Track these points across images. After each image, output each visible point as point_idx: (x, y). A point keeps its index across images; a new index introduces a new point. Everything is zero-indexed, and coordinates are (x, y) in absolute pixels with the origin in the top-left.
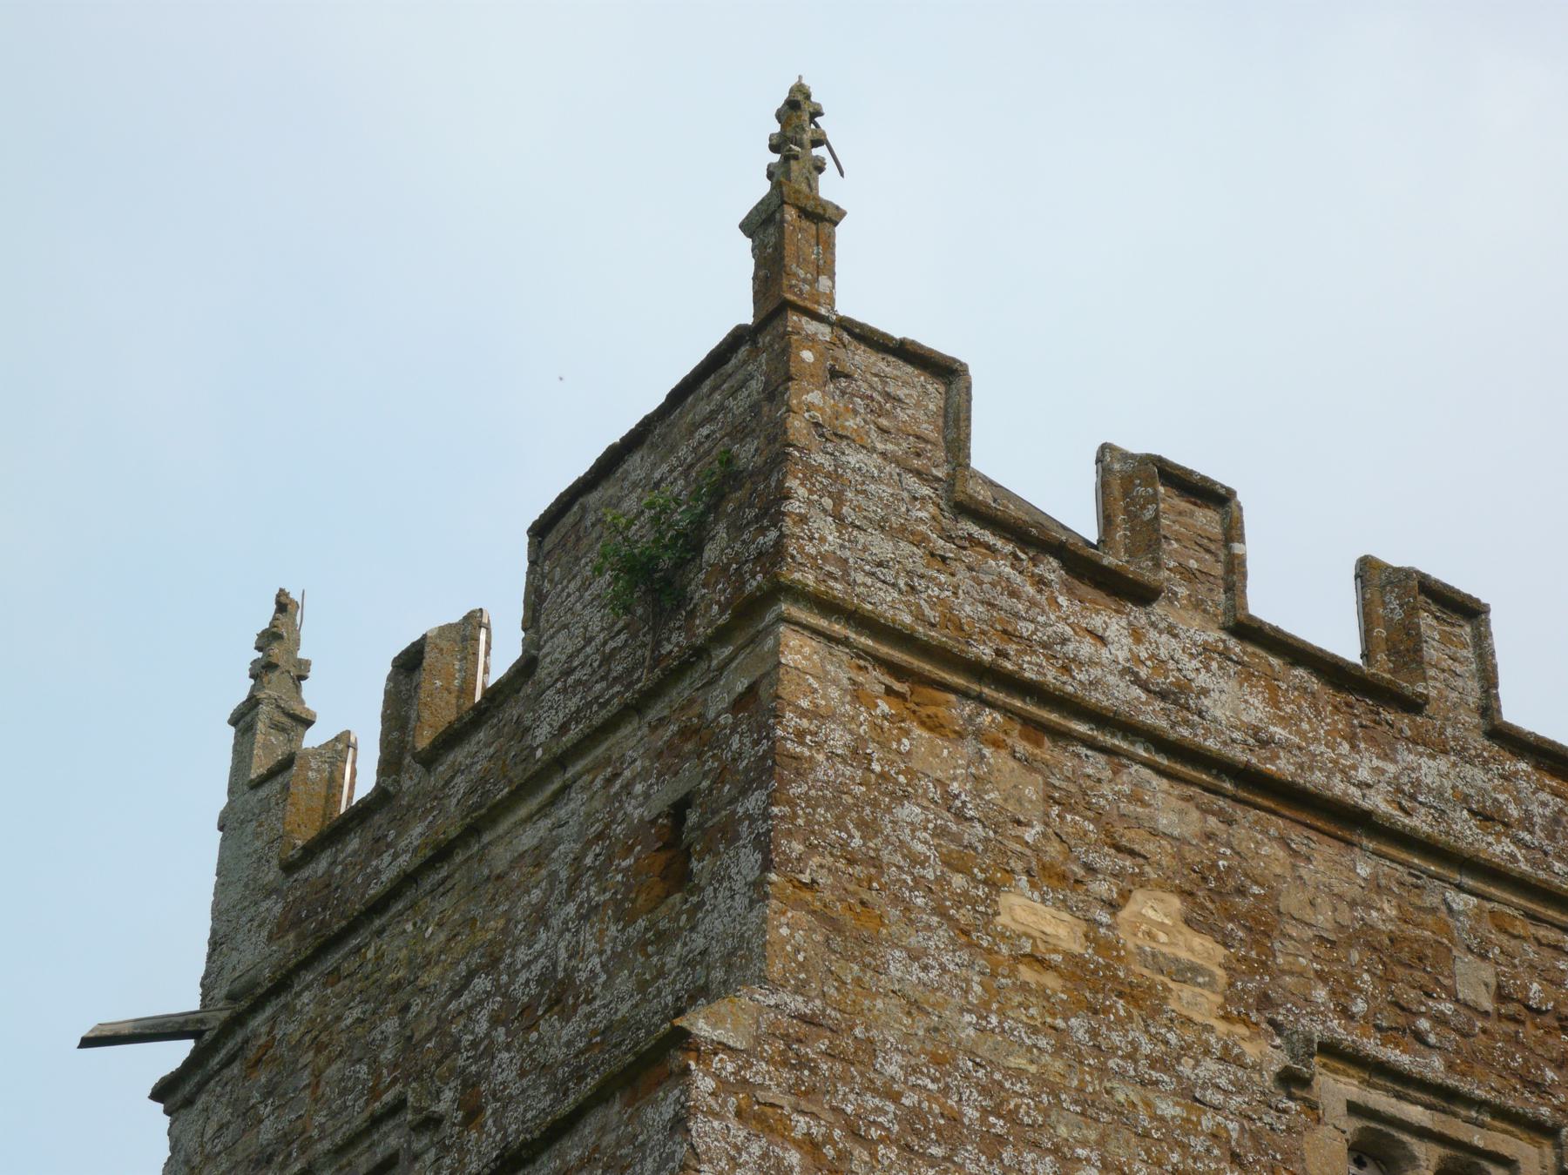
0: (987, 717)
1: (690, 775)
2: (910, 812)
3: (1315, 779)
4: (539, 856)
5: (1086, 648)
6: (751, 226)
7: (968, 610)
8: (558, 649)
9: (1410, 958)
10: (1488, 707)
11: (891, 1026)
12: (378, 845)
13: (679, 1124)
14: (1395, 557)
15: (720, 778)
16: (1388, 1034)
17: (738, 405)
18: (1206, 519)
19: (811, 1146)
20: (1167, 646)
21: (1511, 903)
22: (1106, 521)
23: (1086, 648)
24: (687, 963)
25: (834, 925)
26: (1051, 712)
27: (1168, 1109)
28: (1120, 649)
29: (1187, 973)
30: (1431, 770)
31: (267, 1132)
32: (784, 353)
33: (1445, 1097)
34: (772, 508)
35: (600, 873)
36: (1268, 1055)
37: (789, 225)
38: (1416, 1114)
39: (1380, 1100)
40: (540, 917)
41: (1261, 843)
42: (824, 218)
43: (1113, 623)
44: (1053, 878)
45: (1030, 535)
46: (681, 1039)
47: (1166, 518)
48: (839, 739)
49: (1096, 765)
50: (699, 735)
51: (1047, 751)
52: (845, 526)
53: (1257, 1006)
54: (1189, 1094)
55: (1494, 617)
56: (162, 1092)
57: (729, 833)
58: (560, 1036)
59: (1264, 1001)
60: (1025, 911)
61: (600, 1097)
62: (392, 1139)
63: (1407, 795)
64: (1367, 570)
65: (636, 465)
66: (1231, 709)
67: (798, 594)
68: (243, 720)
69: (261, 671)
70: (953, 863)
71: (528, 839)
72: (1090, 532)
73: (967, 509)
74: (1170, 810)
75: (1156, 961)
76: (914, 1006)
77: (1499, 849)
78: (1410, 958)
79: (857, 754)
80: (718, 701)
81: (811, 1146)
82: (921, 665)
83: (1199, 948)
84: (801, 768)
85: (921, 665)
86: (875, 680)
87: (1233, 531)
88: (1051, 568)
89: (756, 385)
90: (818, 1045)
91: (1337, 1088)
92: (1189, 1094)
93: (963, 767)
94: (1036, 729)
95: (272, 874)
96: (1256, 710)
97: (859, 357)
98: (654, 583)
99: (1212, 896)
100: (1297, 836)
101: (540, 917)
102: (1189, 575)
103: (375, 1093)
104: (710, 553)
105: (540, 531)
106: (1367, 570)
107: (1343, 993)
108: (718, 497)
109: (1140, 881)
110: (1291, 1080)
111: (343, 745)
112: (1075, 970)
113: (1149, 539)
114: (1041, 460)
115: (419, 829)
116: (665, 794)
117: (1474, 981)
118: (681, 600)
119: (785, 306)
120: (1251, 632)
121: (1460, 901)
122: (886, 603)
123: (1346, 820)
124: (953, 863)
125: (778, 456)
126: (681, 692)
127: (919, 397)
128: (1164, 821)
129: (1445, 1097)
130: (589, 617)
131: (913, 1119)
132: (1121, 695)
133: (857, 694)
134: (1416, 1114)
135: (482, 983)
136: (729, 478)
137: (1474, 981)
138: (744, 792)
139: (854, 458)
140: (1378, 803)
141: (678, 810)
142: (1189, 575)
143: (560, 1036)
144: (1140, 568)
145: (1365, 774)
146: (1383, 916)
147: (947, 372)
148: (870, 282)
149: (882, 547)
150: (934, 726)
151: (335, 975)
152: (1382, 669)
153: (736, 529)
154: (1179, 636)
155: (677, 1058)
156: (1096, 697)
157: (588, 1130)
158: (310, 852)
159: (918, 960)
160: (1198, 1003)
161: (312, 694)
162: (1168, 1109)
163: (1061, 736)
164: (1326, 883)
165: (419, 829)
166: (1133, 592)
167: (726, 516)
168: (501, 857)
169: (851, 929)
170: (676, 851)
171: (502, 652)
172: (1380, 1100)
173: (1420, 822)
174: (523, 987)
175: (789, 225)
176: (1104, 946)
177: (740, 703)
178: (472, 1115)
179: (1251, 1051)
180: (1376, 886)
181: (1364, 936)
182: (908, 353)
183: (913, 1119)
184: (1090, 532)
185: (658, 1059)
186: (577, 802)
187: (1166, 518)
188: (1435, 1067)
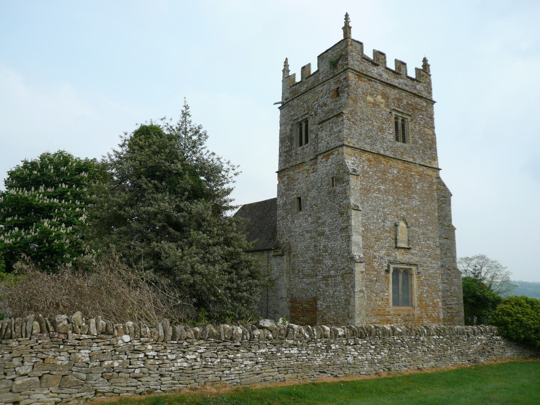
0: (366, 79)
1: (338, 85)
2: (360, 89)
3: (392, 83)
4: (322, 91)
5: (373, 71)
6: (343, 28)
7: (364, 68)
8: (321, 70)
9: (399, 100)
10: (406, 74)
11: (359, 110)
12: (301, 86)
13: (342, 120)
14: (399, 59)
15: (342, 86)
16: (398, 107)
17: (342, 47)
18: (383, 56)
19: (353, 122)
20: (380, 70)
21: (408, 94)
22: (374, 57)
23: (373, 71)
24: (339, 104)
25: (354, 101)
26: (370, 78)
27: (381, 116)
28: (376, 71)
29: (382, 103)
30: (401, 81)
31: (292, 113)
32: (347, 43)
33: (402, 113)
34: (347, 59)
35: (329, 94)
36: (388, 110)
37: (347, 29)
38: (400, 115)
39: (397, 114)
40: (322, 97)
41: (388, 90)
42: (350, 28)
43: (375, 68)
44: (371, 95)
45: (368, 60)
46: (342, 113)
47: (380, 56)
48: (354, 83)
49: (374, 83)
50: (339, 81)
51: (370, 82)
52: (353, 62)
53: (387, 106)
54: (382, 114)
55: (408, 65)
56: (279, 108)
57: (344, 92)
58: (326, 109)
59: (388, 105)
60: (369, 98)
61: (334, 117)
62: (307, 116)
63: (399, 84)
64: (396, 60)
65: (330, 52)
66: (385, 76)
67: (350, 69)
68: (284, 71)
69: (285, 66)
70: (363, 94)
71: (320, 89)
72: (372, 59)
73: (363, 58)
74: (380, 87)
75: (380, 102)
76: (361, 108)
77: (407, 88)
78: (399, 100)
79: (355, 84)
80: (341, 78)
81: (353, 122)
82: (361, 75)
83: (383, 101)
84: (351, 86)
85: (361, 75)
86: (356, 76)
87: (385, 58)
88: (370, 63)
89: (344, 46)
90: (353, 112)
91: (394, 113)
92: (382, 114)
93: (364, 85)
94: (369, 80)
95: (289, 87)
96: (387, 76)
97: (354, 43)
98: (334, 64)
99: (385, 96)
100: (391, 89)
101: (322, 97)
102: (382, 63)
103: (304, 111)
104: (339, 63)
105: (318, 57)
106: (396, 60)
107: (394, 104)
108: (340, 58)
109: (378, 94)
110: (390, 113)
111: (294, 75)
112: (373, 104)
113: (378, 59)
114: (369, 53)
115: (306, 85)
116: (336, 87)
117: (405, 102)
118: (336, 67)
119: (347, 38)
120: (387, 68)
121: (404, 94)
122: (357, 69)
123: (395, 87)
124: (363, 94)
125: (347, 54)
126: (337, 77)
127: (358, 46)
128: (380, 88)
129: (402, 113)
130: (326, 66)
131: (360, 118)
132: (376, 76)
133: (355, 78)
134: (400, 115)
135: (316, 102)
136: (341, 56)
137: (405, 102)
138: (345, 88)
139: (354, 54)
140: (397, 85)
141: (338, 89)
142: (382, 63)
143: (326, 109)
144: (377, 63)
145: (396, 82)
146: (397, 96)
147: (361, 44)
148: (354, 35)
149: (356, 63)
150: (361, 80)
151: (298, 99)
152: (397, 71)
153: (342, 61)
154: (381, 69)
155: (342, 114)
156: (374, 77)
157: (332, 119)
158: (293, 86)
159: (361, 104)
160: (383, 106)
161: (290, 68)
162: (381, 116)
163: (371, 81)
164: (393, 93)
165: (306, 85)
166: (376, 65)
167: (341, 58)
168: (317, 90)
169: (355, 101)
170: (338, 93)
171: (314, 69)
172: (397, 114)
173: (400, 86)
174: (321, 103)
175: (347, 29)
176: (375, 101)
177: (344, 79)
178: (316, 115)
179: (387, 110)
180: (397, 93)
181: (396, 98)
182: (358, 42)
183: (360, 118)
184: (372, 59)
185: (340, 114)
186: (325, 86)
187: (380, 56)
188: (401, 110)
